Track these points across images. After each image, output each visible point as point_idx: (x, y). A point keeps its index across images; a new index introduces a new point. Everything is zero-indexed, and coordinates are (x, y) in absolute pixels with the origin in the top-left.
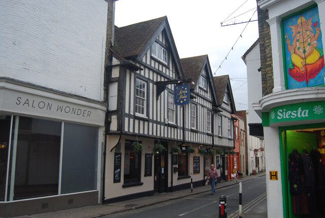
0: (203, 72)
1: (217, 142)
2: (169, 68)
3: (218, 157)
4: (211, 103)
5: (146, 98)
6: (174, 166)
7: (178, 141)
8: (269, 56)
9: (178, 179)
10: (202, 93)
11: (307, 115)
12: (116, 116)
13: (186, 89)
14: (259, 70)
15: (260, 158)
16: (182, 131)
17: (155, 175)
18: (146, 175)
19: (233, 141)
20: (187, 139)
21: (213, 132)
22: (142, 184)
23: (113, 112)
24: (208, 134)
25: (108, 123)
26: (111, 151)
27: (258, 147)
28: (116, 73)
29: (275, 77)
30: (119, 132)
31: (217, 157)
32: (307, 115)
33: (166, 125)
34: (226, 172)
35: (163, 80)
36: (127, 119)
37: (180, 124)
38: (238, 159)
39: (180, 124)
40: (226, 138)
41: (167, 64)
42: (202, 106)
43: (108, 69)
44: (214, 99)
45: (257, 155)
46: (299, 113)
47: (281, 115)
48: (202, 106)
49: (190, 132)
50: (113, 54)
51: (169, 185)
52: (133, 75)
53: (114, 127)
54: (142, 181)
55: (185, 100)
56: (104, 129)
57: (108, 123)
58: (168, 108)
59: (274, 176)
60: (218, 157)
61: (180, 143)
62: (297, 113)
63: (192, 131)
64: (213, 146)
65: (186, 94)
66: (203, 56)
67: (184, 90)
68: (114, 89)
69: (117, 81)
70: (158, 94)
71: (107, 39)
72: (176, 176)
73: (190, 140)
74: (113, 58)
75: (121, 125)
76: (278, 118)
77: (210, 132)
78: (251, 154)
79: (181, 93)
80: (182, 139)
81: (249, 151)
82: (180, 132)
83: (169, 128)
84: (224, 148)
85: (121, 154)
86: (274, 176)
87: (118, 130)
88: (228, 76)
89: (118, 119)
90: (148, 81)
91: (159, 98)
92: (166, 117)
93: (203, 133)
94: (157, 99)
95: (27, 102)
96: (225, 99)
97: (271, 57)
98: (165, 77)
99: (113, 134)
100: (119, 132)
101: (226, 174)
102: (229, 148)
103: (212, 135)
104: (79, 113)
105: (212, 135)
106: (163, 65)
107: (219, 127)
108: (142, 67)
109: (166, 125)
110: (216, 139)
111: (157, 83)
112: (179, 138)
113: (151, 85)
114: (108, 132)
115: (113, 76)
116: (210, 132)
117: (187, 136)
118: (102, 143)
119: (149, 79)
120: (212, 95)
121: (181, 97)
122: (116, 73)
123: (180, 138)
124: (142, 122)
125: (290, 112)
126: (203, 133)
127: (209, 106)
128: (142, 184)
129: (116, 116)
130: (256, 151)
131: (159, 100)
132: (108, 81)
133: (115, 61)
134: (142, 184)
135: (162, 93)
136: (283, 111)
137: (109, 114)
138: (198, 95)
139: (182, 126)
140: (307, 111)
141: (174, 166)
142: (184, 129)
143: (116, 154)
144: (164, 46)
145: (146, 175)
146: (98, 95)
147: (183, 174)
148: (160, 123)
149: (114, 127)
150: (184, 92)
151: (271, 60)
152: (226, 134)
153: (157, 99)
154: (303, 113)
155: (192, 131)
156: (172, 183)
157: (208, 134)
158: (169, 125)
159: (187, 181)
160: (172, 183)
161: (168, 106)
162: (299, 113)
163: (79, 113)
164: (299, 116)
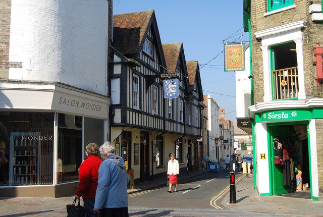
2: (154, 61)
8: (261, 72)
11: (287, 117)
12: (120, 110)
14: (249, 77)
19: (199, 130)
21: (184, 121)
23: (117, 106)
24: (181, 123)
25: (111, 116)
27: (218, 136)
28: (117, 70)
29: (265, 83)
30: (124, 124)
32: (287, 117)
35: (154, 74)
36: (128, 112)
37: (162, 115)
41: (152, 56)
43: (111, 65)
44: (186, 88)
45: (217, 144)
46: (282, 116)
47: (271, 116)
50: (115, 52)
51: (151, 174)
52: (131, 70)
53: (118, 119)
55: (174, 94)
57: (111, 116)
58: (133, 92)
59: (263, 156)
62: (281, 116)
64: (185, 135)
68: (116, 83)
69: (119, 77)
70: (148, 86)
71: (109, 36)
74: (115, 55)
75: (124, 118)
76: (269, 118)
78: (212, 143)
79: (170, 86)
86: (263, 156)
87: (121, 122)
90: (140, 75)
92: (152, 108)
95: (83, 105)
97: (262, 73)
98: (153, 71)
99: (118, 126)
100: (124, 124)
103: (184, 124)
104: (87, 107)
106: (148, 56)
108: (139, 64)
111: (146, 77)
114: (112, 124)
115: (115, 73)
116: (182, 121)
118: (108, 134)
119: (141, 73)
122: (117, 70)
125: (277, 115)
129: (120, 110)
130: (216, 139)
132: (111, 76)
133: (117, 59)
135: (149, 88)
136: (272, 114)
137: (112, 108)
140: (287, 115)
146: (103, 90)
149: (118, 119)
150: (173, 86)
151: (263, 76)
153: (146, 93)
154: (285, 116)
157: (181, 123)
160: (153, 171)
161: (133, 89)
162: (282, 116)
163: (87, 107)
164: (282, 117)
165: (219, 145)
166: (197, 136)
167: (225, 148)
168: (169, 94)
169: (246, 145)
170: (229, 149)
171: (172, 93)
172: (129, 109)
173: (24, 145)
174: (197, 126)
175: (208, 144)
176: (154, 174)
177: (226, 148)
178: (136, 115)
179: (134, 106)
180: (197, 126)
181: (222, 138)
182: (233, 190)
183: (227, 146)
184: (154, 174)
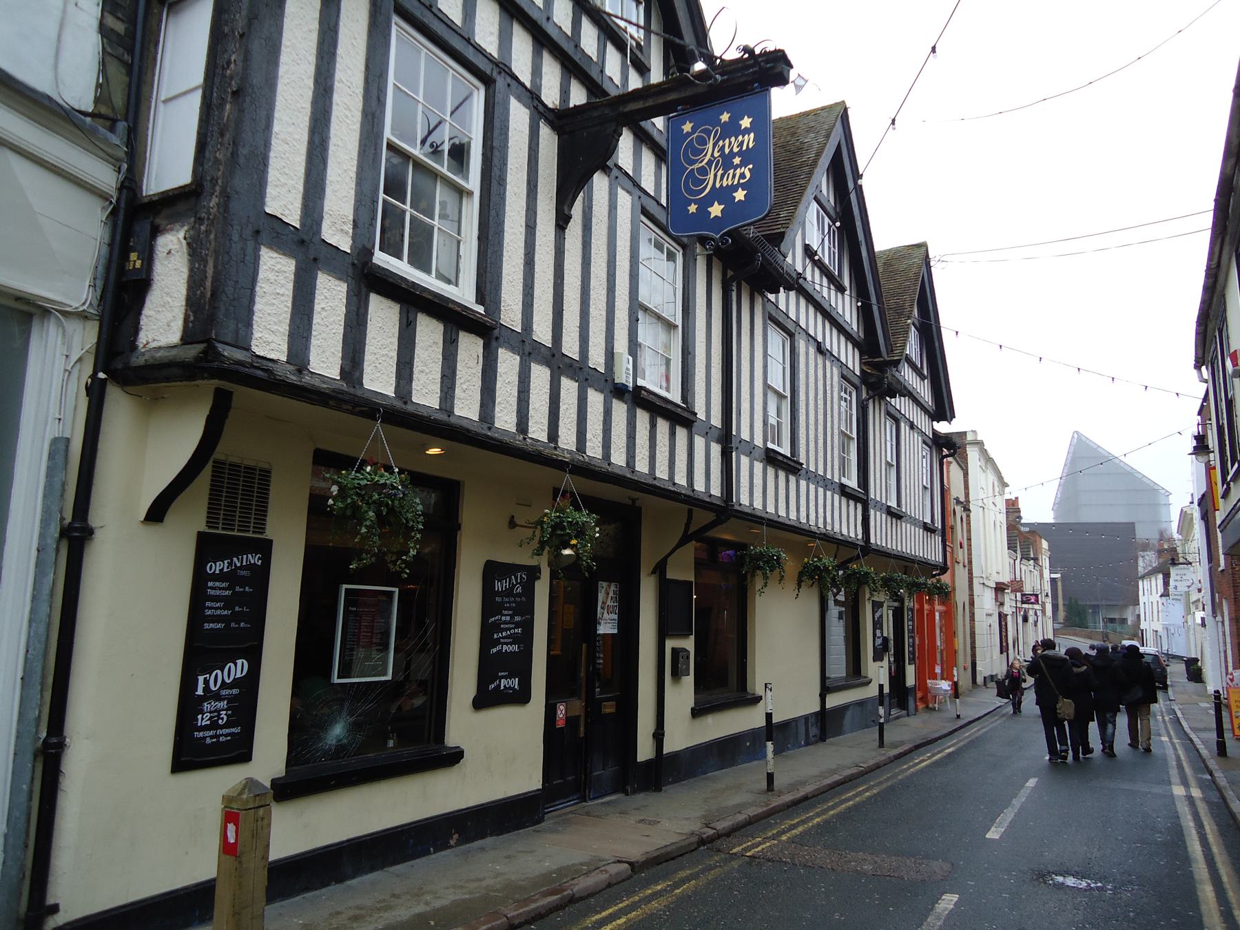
0: (822, 183)
1: (883, 535)
3: (880, 605)
4: (856, 344)
5: (474, 182)
6: (670, 644)
7: (690, 501)
9: (697, 713)
10: (814, 279)
13: (746, 122)
15: (1009, 618)
16: (716, 449)
17: (554, 692)
18: (485, 700)
20: (745, 500)
21: (488, 285)
22: (455, 757)
24: (844, 491)
26: (157, 513)
27: (1006, 578)
31: (877, 606)
33: (619, 392)
34: (910, 671)
38: (949, 616)
39: (708, 407)
40: (914, 522)
42: (820, 349)
45: (1002, 604)
48: (820, 349)
49: (758, 467)
51: (645, 751)
54: (453, 738)
55: (740, 195)
56: (85, 338)
60: (880, 605)
61: (707, 517)
63: (771, 458)
64: (866, 549)
65: (746, 157)
66: (823, 109)
67: (732, 129)
72: (682, 695)
73: (758, 504)
77: (852, 482)
78: (986, 601)
79: (710, 151)
80: (716, 491)
81: (977, 588)
82: (707, 453)
83: (642, 417)
84: (907, 563)
85: (265, 548)
87: (187, 338)
88: (923, 246)
89: (195, 249)
91: (577, 210)
92: (621, 345)
93: (824, 483)
94: (562, 221)
96: (912, 347)
101: (910, 681)
102: (926, 567)
103: (859, 497)
105: (859, 497)
107: (889, 465)
109: (619, 392)
110: (877, 519)
112: (699, 486)
113: (518, 116)
116: (852, 482)
117: (745, 406)
120: (865, 313)
121: (712, 180)
123: (707, 484)
124: (429, 332)
126: (824, 483)
127: (851, 358)
128: (455, 757)
130: (1000, 589)
131: (574, 230)
134: (456, 756)
138: (795, 284)
139: (716, 421)
141: (670, 644)
142: (726, 438)
143: (207, 547)
144: (661, 216)
145: (485, 700)
147: (722, 681)
148: (578, 370)
150: (732, 144)
152: (918, 505)
153: (562, 221)
155: (771, 458)
156: (659, 736)
157: (844, 491)
158: (639, 399)
159: (747, 720)
160: (659, 736)
165: (1007, 609)
166: (935, 567)
167: (1025, 619)
168: (705, 204)
169: (867, 583)
170: (1039, 623)
171: (723, 194)
172: (750, 449)
173: (212, 588)
174: (928, 520)
175: (972, 603)
176: (668, 748)
177: (1031, 619)
178: (787, 481)
179: (843, 478)
180: (928, 520)
181: (1016, 585)
182: (1166, 584)
183: (1031, 613)
184: (668, 748)
